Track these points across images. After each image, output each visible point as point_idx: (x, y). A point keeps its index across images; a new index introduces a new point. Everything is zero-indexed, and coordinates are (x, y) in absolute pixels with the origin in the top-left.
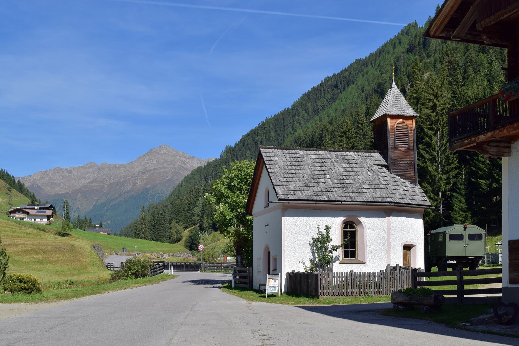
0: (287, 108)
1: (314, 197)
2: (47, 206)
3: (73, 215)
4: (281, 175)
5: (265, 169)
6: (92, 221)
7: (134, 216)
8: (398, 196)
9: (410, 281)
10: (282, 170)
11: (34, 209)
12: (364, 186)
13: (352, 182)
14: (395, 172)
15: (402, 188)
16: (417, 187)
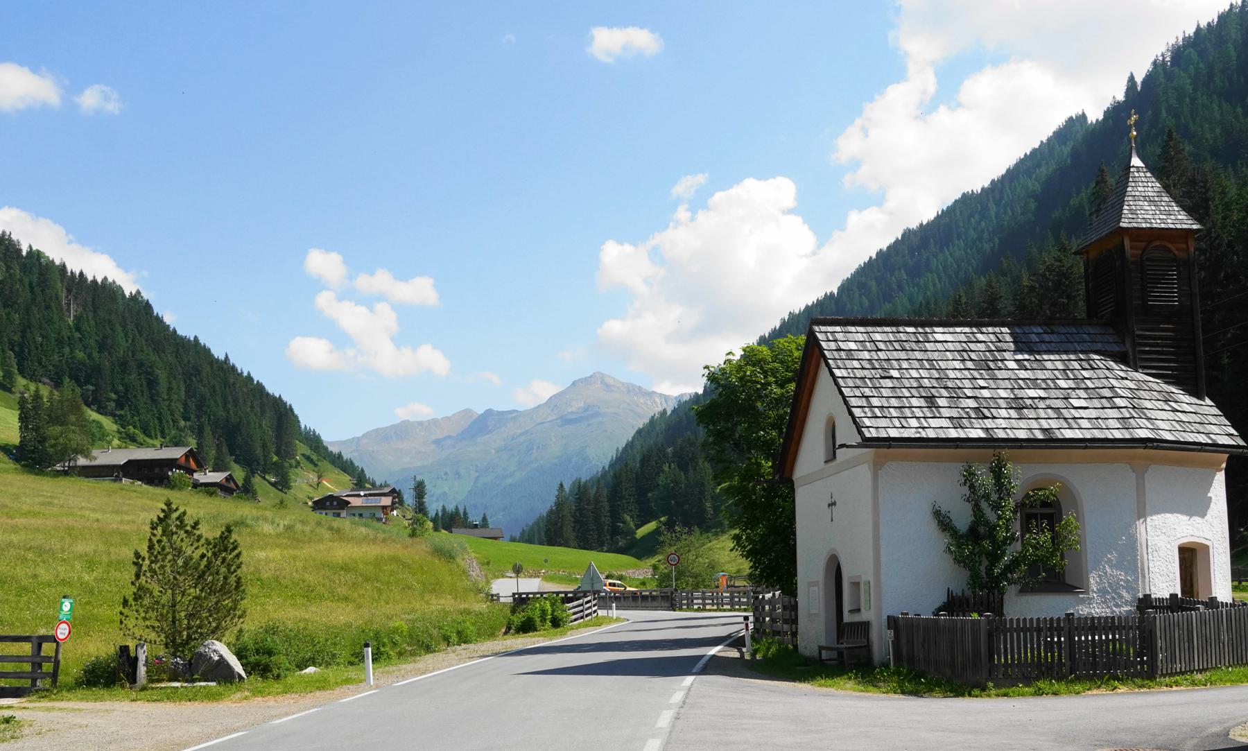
0: (831, 293)
1: (952, 431)
2: (387, 490)
3: (433, 507)
4: (865, 383)
5: (824, 371)
6: (469, 515)
7: (544, 504)
8: (1161, 425)
9: (1233, 643)
10: (883, 352)
11: (359, 496)
12: (1076, 403)
13: (1042, 393)
14: (1144, 367)
15: (1170, 406)
16: (1203, 403)
